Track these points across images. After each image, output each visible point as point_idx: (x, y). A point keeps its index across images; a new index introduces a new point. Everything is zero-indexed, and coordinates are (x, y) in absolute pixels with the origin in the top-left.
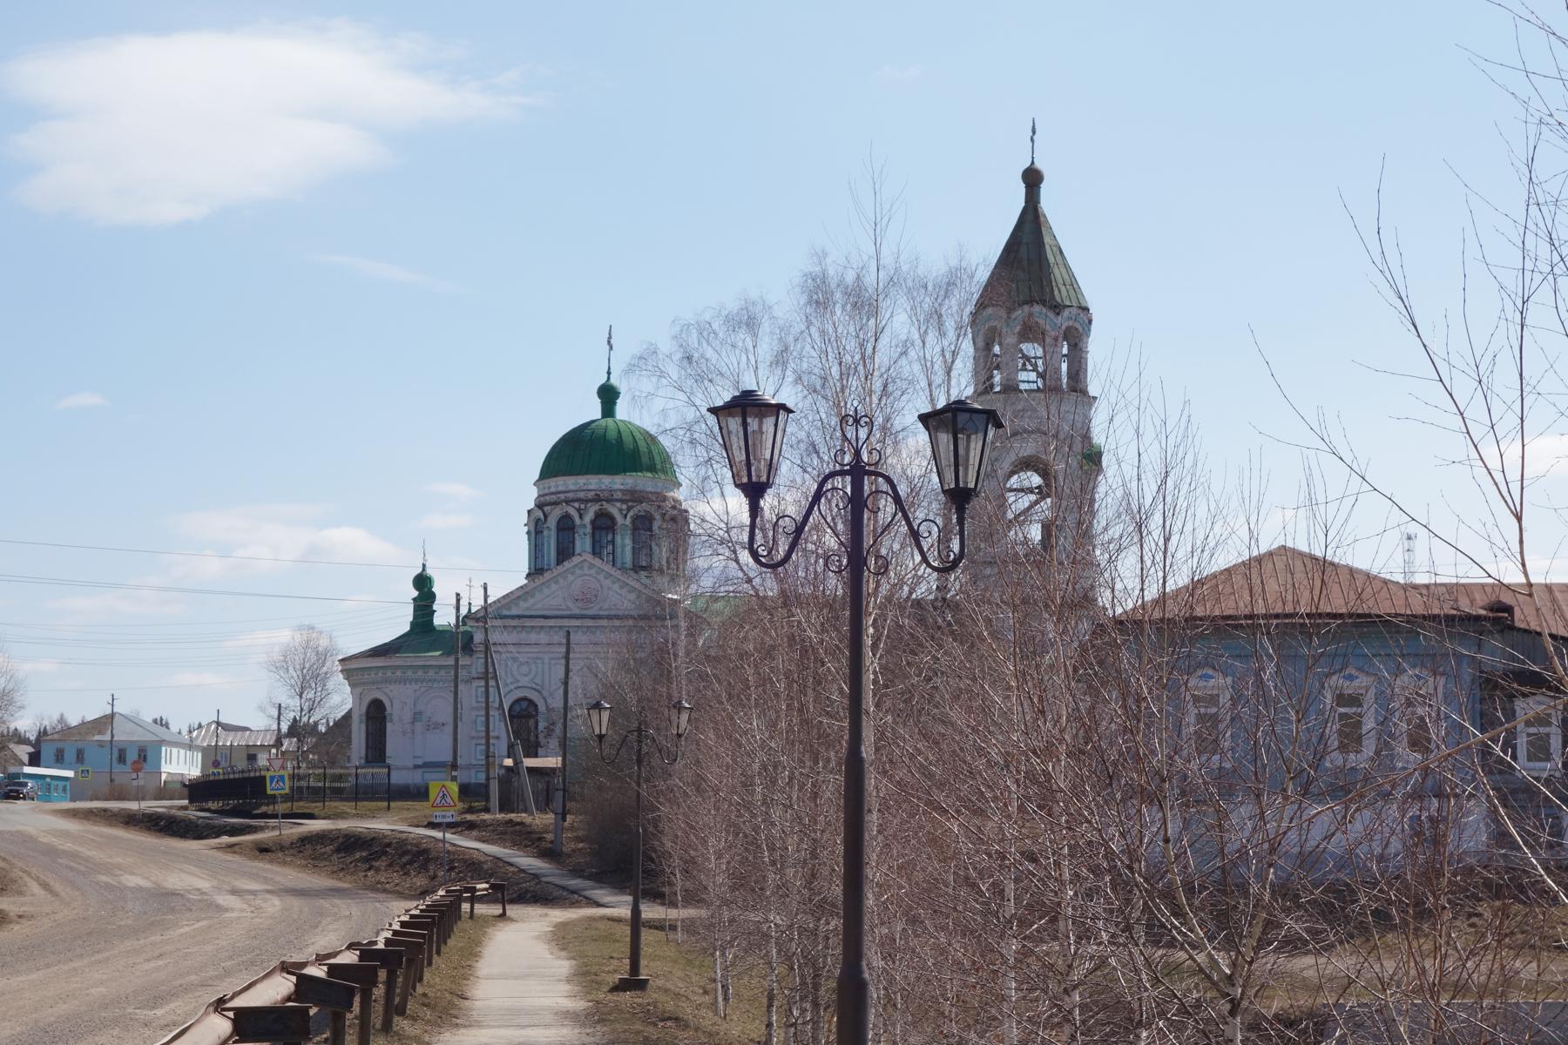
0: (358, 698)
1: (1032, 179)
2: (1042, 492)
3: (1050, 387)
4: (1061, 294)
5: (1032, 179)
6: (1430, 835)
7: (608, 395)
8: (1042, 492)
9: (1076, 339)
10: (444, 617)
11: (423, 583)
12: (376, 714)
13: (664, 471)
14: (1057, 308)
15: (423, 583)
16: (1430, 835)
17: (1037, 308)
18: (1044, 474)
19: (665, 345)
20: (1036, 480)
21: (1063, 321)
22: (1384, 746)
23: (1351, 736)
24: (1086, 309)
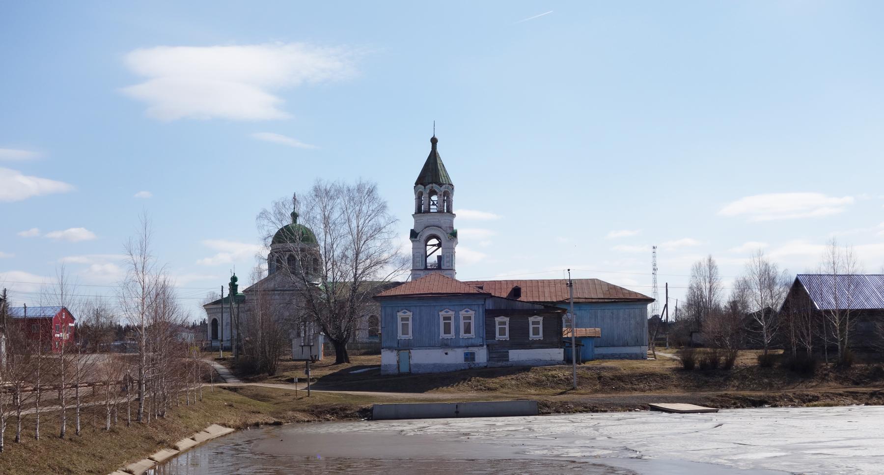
0: (209, 318)
1: (434, 141)
2: (439, 245)
3: (440, 212)
4: (442, 180)
5: (434, 141)
6: (470, 357)
7: (295, 216)
8: (439, 245)
9: (447, 196)
10: (240, 291)
11: (234, 279)
12: (214, 323)
13: (312, 241)
14: (441, 185)
15: (234, 279)
16: (470, 357)
17: (434, 185)
18: (438, 238)
19: (270, 209)
20: (434, 241)
21: (443, 189)
22: (457, 332)
23: (447, 330)
24: (452, 185)
